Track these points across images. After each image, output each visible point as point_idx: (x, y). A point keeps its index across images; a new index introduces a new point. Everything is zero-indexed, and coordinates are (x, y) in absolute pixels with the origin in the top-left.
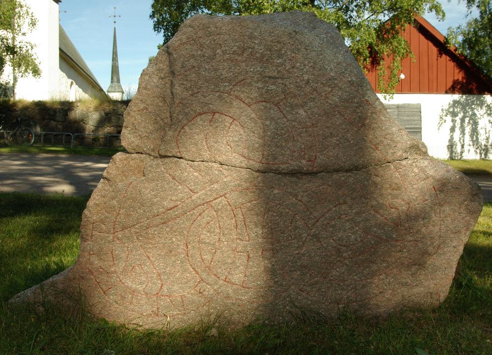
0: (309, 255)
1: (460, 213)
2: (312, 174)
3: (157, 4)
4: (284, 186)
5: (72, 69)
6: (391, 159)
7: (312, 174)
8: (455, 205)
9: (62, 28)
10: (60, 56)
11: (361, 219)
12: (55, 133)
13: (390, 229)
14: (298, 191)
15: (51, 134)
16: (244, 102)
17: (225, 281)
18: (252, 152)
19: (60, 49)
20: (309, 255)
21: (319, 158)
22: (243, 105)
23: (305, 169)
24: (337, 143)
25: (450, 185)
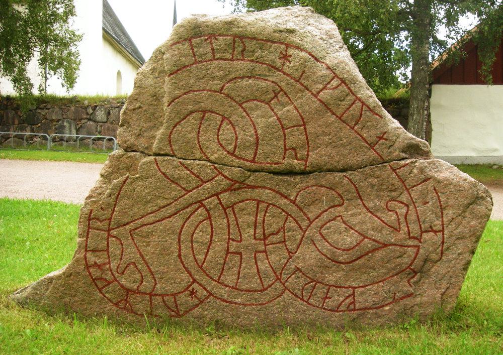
0: (304, 258)
1: (464, 218)
2: (304, 173)
3: (7, 138)
4: (276, 185)
5: (118, 53)
6: (387, 159)
7: (304, 173)
8: (459, 209)
9: (107, 3)
10: (104, 37)
11: (357, 221)
12: (94, 137)
13: (388, 232)
14: (291, 191)
15: (90, 138)
16: (234, 100)
17: (218, 282)
18: (243, 151)
19: (103, 29)
20: (304, 258)
21: (311, 157)
22: (234, 103)
23: (297, 168)
24: (330, 141)
25: (452, 186)
